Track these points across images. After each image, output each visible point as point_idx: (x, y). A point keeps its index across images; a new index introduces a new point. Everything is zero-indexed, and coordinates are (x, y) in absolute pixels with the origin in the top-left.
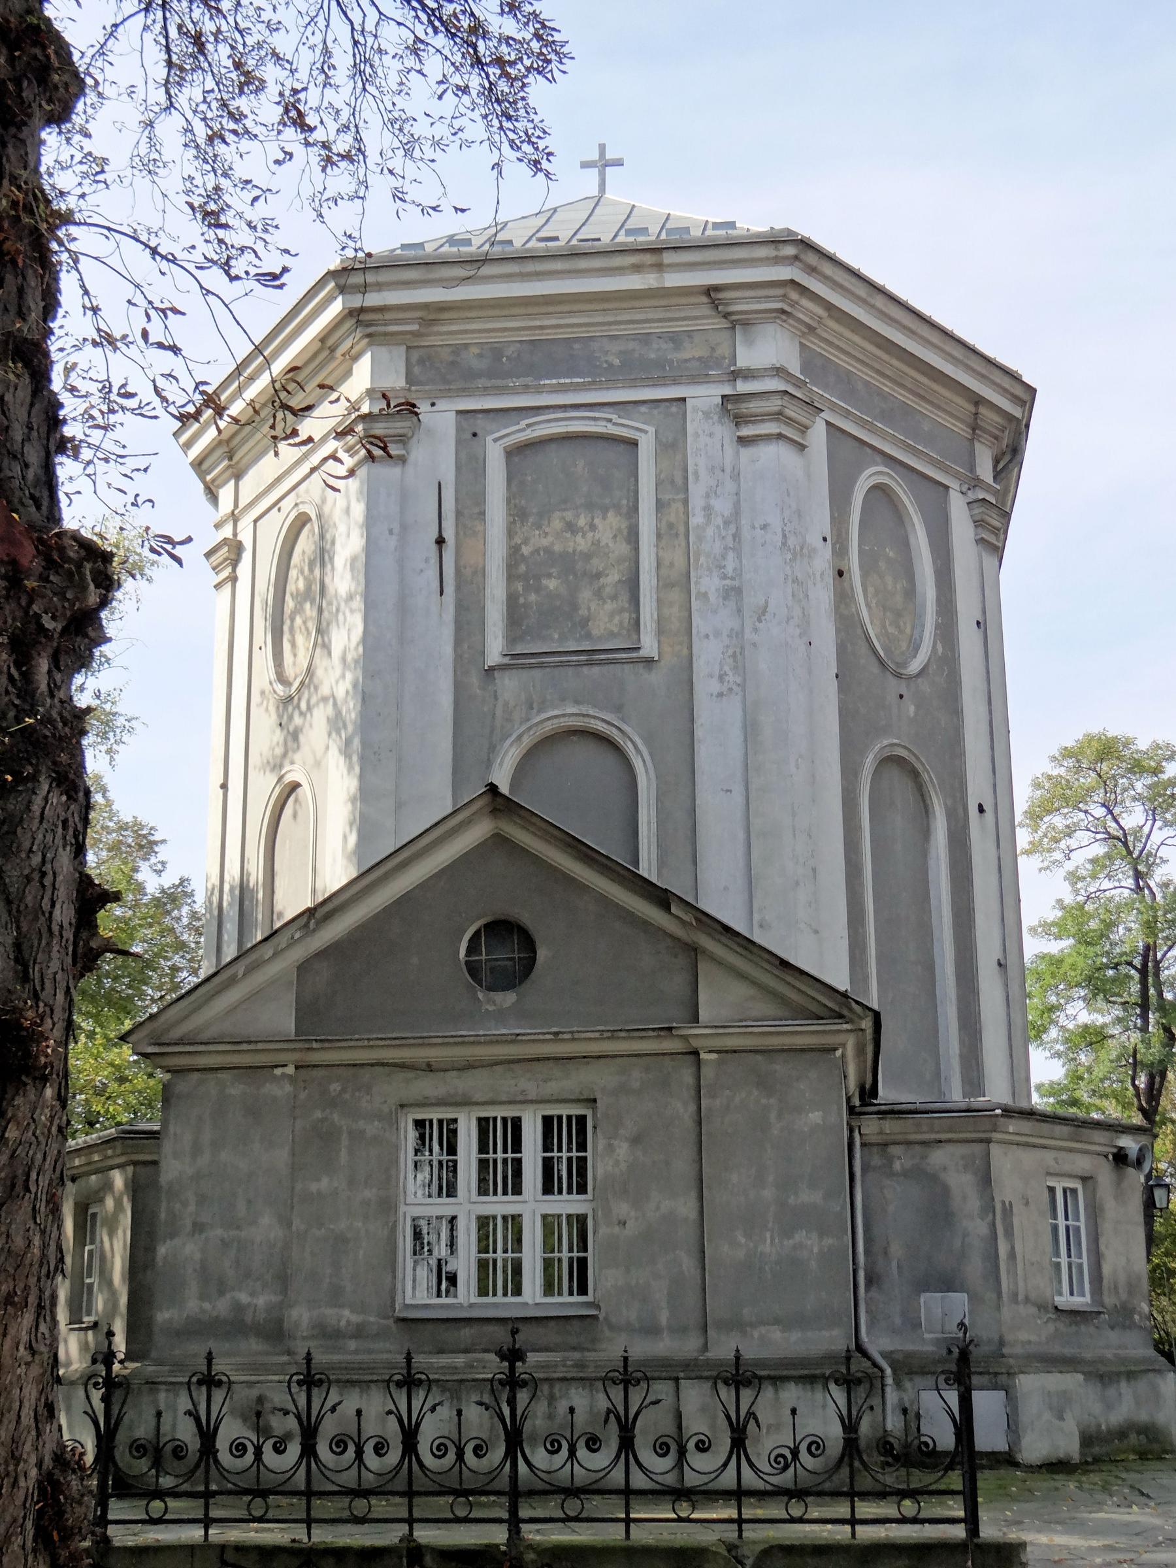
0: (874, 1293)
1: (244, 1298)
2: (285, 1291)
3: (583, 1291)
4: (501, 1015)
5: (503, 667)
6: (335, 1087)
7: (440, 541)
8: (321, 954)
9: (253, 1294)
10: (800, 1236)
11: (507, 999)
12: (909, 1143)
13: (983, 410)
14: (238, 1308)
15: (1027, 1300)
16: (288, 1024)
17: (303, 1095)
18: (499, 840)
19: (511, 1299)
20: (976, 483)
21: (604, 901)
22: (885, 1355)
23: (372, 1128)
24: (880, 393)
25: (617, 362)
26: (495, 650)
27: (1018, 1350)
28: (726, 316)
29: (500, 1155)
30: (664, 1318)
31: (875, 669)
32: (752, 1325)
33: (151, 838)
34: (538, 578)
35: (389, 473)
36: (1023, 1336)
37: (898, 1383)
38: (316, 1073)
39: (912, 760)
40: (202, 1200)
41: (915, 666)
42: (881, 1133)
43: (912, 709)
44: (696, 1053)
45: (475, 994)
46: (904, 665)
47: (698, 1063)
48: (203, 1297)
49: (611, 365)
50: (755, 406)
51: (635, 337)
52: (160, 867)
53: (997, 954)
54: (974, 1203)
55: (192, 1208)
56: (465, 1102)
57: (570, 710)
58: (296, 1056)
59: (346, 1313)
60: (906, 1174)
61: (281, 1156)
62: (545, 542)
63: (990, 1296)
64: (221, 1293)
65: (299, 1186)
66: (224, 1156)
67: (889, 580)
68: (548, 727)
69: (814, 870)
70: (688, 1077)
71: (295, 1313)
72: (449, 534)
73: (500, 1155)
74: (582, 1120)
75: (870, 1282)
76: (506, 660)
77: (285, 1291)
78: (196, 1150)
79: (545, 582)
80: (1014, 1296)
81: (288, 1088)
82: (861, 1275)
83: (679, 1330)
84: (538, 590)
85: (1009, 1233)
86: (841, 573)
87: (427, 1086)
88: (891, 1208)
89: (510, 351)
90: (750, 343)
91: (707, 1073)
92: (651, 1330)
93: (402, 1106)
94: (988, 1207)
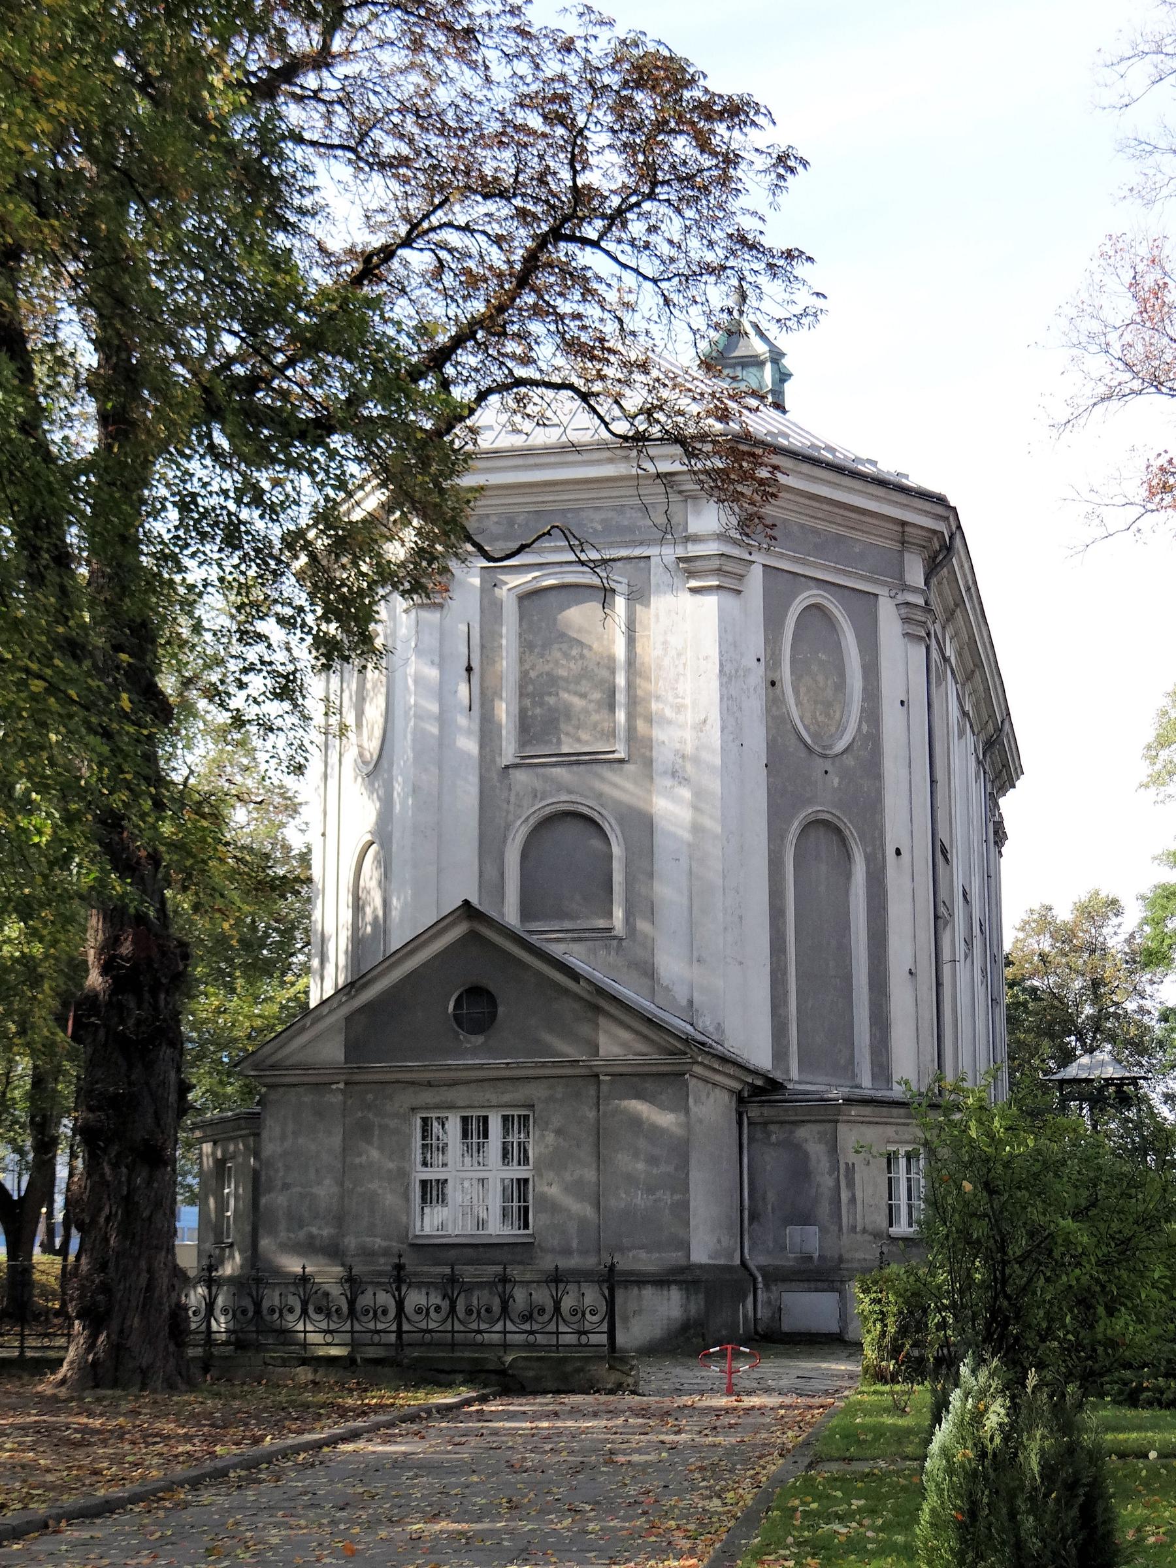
0: (755, 1225)
1: (314, 1230)
2: (340, 1227)
3: (526, 1226)
4: (475, 1051)
5: (516, 766)
6: (370, 1097)
7: (469, 669)
8: (360, 1010)
9: (320, 1228)
10: (659, 1194)
11: (479, 1039)
12: (782, 1123)
13: (907, 529)
14: (311, 1237)
15: (864, 1231)
16: (340, 1056)
17: (350, 1102)
18: (472, 935)
19: (522, 1232)
20: (906, 588)
21: (539, 974)
22: (759, 1268)
23: (393, 1123)
24: (815, 531)
25: (599, 528)
26: (509, 751)
27: (855, 1265)
28: (680, 492)
29: (475, 1140)
30: (574, 1245)
31: (803, 754)
32: (630, 1249)
33: (296, 801)
34: (542, 696)
35: (432, 617)
36: (859, 1255)
37: (767, 1287)
38: (357, 1088)
39: (835, 821)
40: (288, 1168)
41: (840, 746)
42: (762, 1115)
43: (836, 781)
44: (597, 1076)
45: (458, 1034)
46: (830, 747)
47: (599, 1083)
48: (288, 1230)
49: (595, 530)
50: (698, 565)
51: (614, 508)
52: (303, 827)
53: (909, 965)
54: (824, 1165)
55: (281, 1174)
56: (451, 1107)
57: (564, 798)
58: (343, 1077)
59: (378, 1240)
60: (778, 1144)
61: (336, 1141)
62: (547, 668)
63: (835, 1228)
64: (301, 1227)
65: (348, 1159)
66: (301, 1141)
67: (820, 679)
68: (548, 810)
69: (741, 917)
70: (592, 1092)
71: (346, 1240)
72: (475, 664)
73: (475, 1140)
74: (526, 1117)
75: (752, 1218)
76: (518, 761)
77: (340, 1227)
78: (283, 1138)
79: (547, 698)
80: (853, 1229)
81: (340, 1097)
82: (746, 1213)
83: (584, 1252)
84: (542, 704)
85: (851, 1185)
86: (773, 684)
87: (428, 1097)
88: (768, 1168)
89: (521, 519)
90: (698, 513)
91: (604, 1088)
92: (567, 1252)
93: (413, 1109)
94: (835, 1167)
